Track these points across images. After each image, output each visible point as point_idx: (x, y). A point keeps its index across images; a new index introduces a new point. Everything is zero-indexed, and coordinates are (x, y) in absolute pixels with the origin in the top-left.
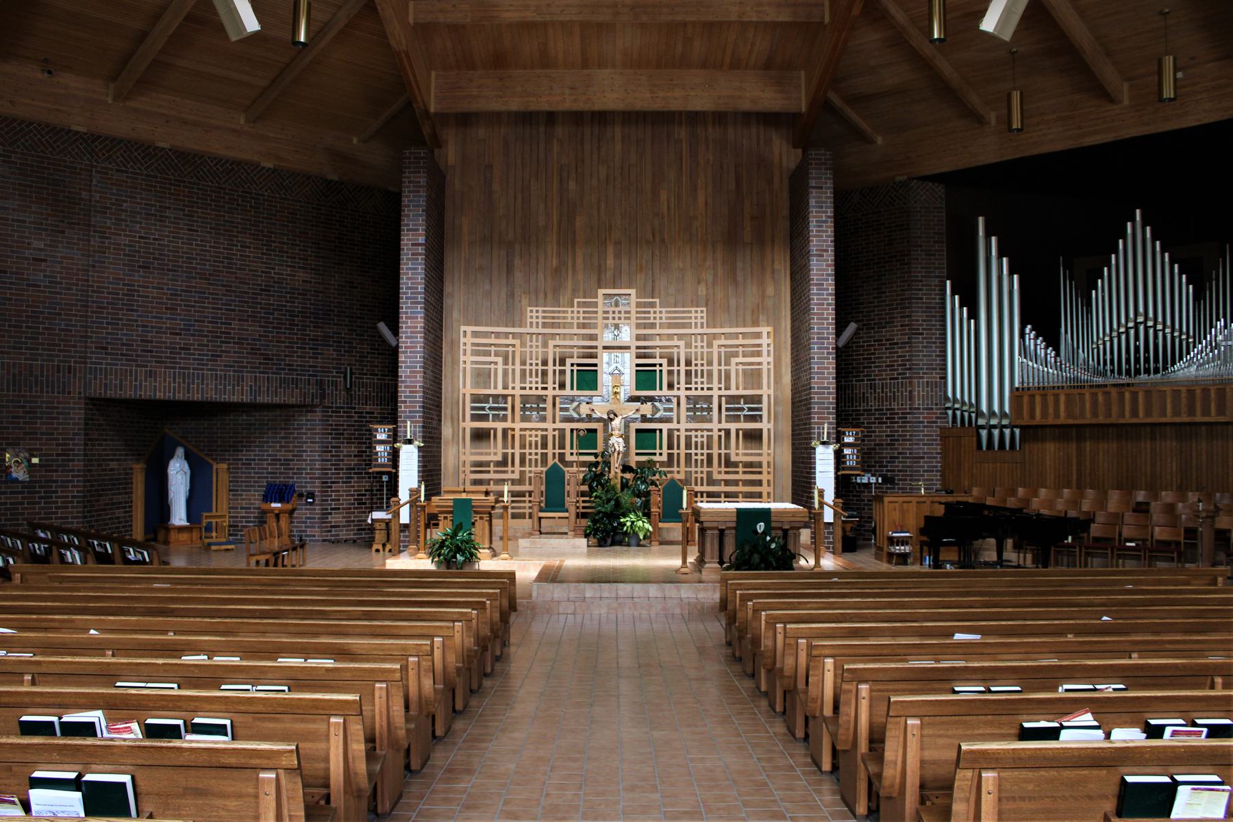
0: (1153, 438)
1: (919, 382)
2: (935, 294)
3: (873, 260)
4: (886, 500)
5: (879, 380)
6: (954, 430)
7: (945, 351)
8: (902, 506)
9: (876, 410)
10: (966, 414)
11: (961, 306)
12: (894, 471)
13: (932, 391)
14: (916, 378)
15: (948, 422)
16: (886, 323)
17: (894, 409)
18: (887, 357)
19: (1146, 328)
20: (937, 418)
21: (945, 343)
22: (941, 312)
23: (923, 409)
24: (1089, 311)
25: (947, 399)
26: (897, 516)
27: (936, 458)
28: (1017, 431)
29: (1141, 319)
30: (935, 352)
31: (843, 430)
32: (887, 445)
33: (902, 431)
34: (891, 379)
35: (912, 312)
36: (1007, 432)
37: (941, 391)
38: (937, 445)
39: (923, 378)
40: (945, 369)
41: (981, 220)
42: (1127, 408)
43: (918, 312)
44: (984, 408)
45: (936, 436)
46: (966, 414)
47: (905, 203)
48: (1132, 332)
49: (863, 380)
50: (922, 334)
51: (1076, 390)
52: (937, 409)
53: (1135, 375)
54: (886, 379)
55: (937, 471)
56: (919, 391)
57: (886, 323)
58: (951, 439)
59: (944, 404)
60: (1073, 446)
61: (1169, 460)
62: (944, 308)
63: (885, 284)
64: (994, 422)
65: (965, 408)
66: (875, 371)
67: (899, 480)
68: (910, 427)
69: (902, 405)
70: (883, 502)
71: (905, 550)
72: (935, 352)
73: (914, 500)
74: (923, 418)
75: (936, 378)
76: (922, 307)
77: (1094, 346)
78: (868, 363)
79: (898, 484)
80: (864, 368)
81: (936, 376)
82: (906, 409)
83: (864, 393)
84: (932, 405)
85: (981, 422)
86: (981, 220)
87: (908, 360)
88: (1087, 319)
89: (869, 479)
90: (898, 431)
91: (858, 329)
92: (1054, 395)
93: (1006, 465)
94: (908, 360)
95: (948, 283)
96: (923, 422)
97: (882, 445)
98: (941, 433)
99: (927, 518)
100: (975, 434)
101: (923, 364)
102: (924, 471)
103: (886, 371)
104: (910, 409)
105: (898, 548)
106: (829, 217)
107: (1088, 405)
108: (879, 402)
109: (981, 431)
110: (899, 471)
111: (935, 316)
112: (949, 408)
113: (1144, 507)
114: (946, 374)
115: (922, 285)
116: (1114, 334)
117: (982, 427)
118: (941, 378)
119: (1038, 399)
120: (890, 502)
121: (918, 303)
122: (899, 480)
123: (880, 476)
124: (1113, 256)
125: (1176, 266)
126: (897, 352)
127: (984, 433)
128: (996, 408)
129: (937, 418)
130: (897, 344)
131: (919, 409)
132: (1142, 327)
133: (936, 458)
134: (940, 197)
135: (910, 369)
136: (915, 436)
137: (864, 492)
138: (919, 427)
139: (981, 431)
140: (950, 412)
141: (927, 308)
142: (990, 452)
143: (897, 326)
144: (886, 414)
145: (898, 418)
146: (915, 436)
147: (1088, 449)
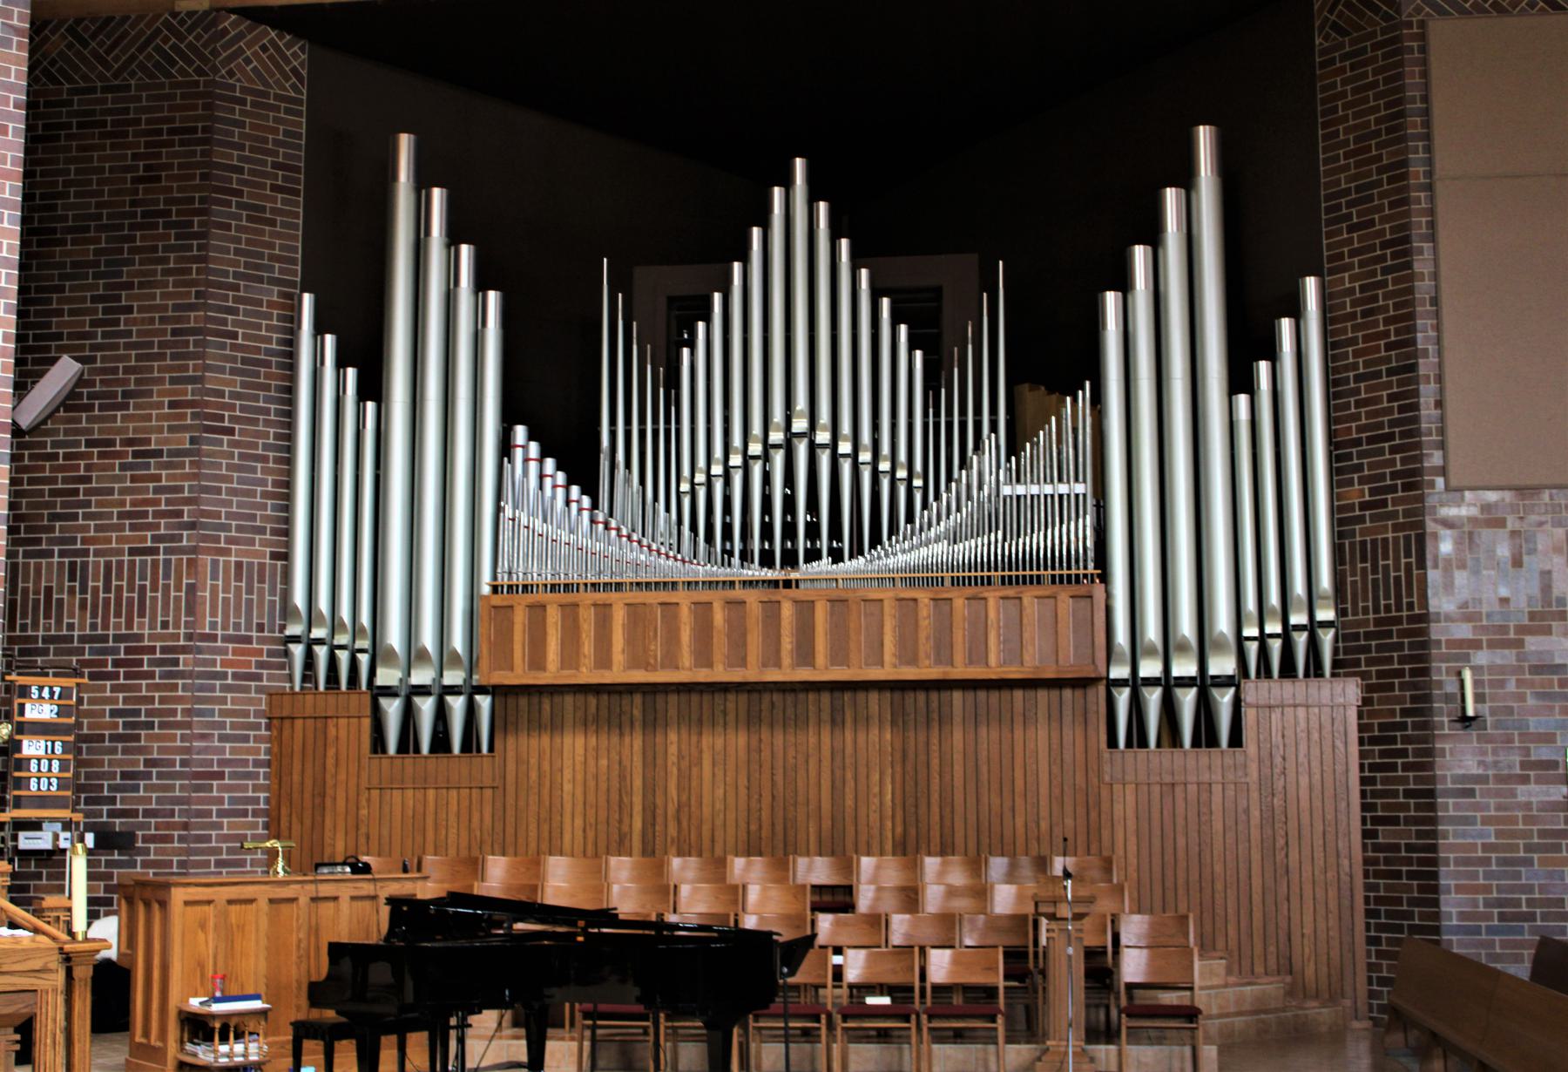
0: (836, 722)
1: (215, 563)
2: (269, 328)
3: (99, 217)
4: (178, 895)
5: (97, 553)
6: (309, 698)
7: (288, 484)
8: (226, 915)
9: (83, 639)
10: (343, 656)
11: (341, 364)
12: (134, 813)
13: (250, 591)
14: (208, 551)
15: (290, 678)
16: (126, 394)
17: (139, 637)
18: (123, 491)
19: (813, 448)
20: (261, 665)
21: (289, 462)
22: (283, 378)
23: (226, 639)
24: (673, 400)
25: (288, 611)
26: (208, 944)
27: (255, 776)
28: (484, 702)
29: (800, 425)
30: (263, 483)
31: (22, 680)
32: (113, 738)
33: (163, 700)
34: (132, 552)
35: (207, 368)
36: (457, 704)
37: (273, 592)
38: (257, 739)
39: (227, 552)
40: (287, 532)
41: (405, 142)
42: (787, 644)
43: (222, 370)
44: (394, 637)
45: (258, 714)
46: (343, 656)
47: (200, 72)
48: (778, 458)
49: (50, 554)
50: (231, 431)
51: (654, 593)
52: (261, 640)
53: (807, 561)
54: (119, 552)
55: (256, 813)
56: (214, 589)
57: (126, 394)
58: (299, 723)
59: (283, 628)
60: (636, 742)
61: (876, 777)
62: (291, 367)
63: (129, 286)
64: (422, 676)
65: (342, 639)
66: (86, 528)
67: (146, 839)
68: (185, 688)
69: (165, 625)
70: (164, 904)
71: (245, 1055)
72: (263, 483)
73: (263, 893)
74: (224, 663)
75: (262, 555)
76: (234, 359)
77: (685, 487)
78: (64, 505)
79: (146, 852)
80: (55, 517)
81: (262, 548)
82: (176, 637)
83: (49, 590)
84: (249, 628)
85: (387, 676)
86: (405, 142)
87: (188, 501)
88: (667, 421)
89: (56, 837)
90: (151, 700)
91: (80, 381)
92: (595, 605)
93: (454, 793)
94: (188, 501)
95: (307, 299)
96: (224, 676)
97: (101, 738)
98: (270, 704)
99: (336, 950)
100: (368, 711)
101: (229, 516)
102: (221, 813)
103: (121, 528)
104: (189, 637)
105: (224, 1048)
106: (18, 32)
107: (686, 635)
108: (94, 615)
109: (383, 702)
110: (147, 813)
111: (267, 388)
112: (295, 639)
113: (840, 898)
114: (289, 545)
115: (237, 300)
116: (736, 460)
117: (389, 692)
118: (274, 556)
119: (553, 616)
120: (187, 903)
121: (223, 346)
122: (146, 839)
123: (88, 828)
124: (737, 266)
125: (885, 303)
126: (158, 478)
127: (392, 709)
128: (428, 639)
129: (261, 665)
130: (158, 453)
131: (213, 638)
132: (802, 449)
133: (255, 776)
134: (295, 71)
135: (192, 526)
136: (201, 713)
137: (39, 876)
138: (213, 689)
139: (383, 702)
140: (298, 650)
141: (244, 361)
142: (409, 759)
143: (160, 405)
144: (115, 651)
145: (152, 663)
146: (201, 713)
147: (673, 749)
